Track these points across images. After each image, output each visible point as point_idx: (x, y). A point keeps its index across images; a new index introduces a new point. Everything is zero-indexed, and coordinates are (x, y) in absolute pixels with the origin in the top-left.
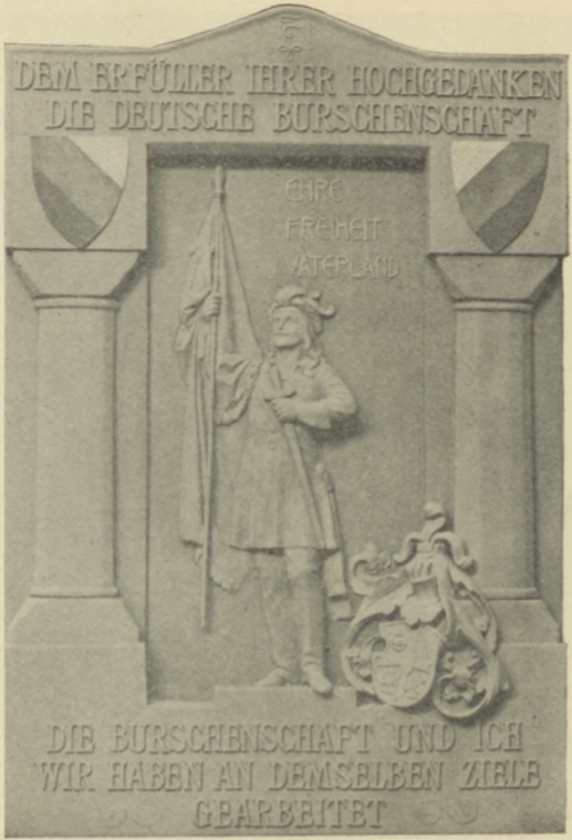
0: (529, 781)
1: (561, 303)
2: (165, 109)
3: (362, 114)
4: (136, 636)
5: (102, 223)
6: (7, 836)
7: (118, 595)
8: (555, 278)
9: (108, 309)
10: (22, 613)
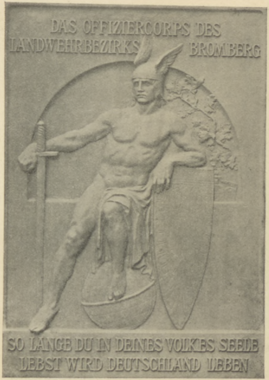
0: (218, 368)
2: (133, 362)
3: (154, 364)
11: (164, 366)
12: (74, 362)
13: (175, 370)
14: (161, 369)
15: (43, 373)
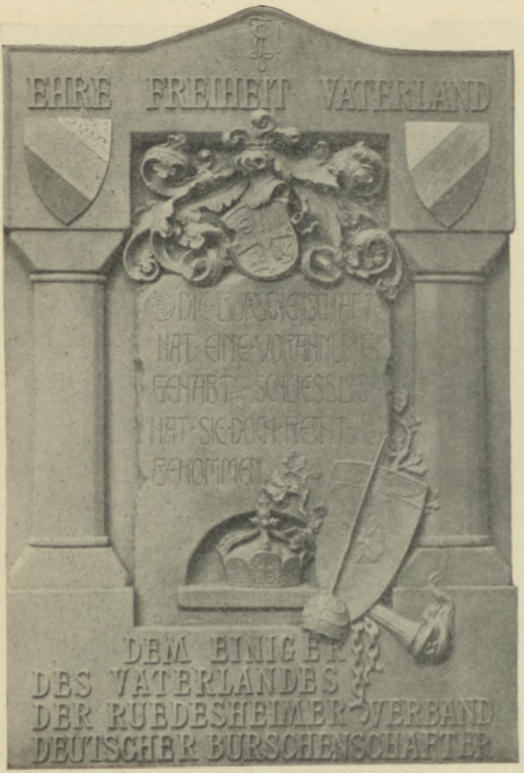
1: (507, 286)
4: (123, 582)
5: (91, 196)
6: (10, 767)
7: (109, 544)
8: (503, 256)
9: (98, 282)
10: (19, 564)
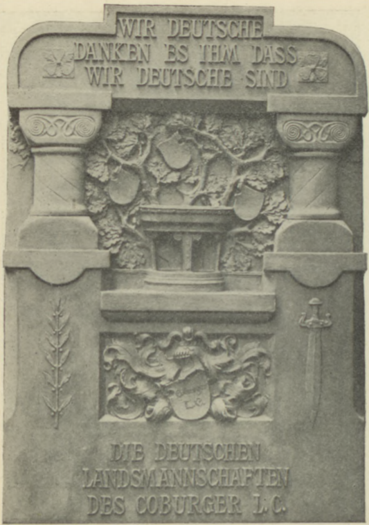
11: (247, 31)
12: (97, 72)
13: (94, 486)
14: (242, 35)
15: (227, 517)
